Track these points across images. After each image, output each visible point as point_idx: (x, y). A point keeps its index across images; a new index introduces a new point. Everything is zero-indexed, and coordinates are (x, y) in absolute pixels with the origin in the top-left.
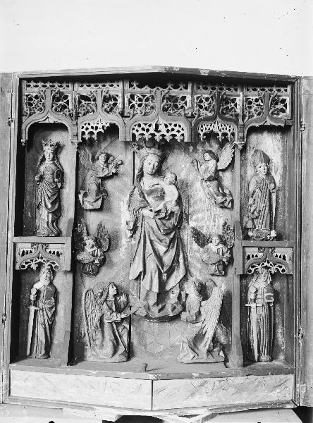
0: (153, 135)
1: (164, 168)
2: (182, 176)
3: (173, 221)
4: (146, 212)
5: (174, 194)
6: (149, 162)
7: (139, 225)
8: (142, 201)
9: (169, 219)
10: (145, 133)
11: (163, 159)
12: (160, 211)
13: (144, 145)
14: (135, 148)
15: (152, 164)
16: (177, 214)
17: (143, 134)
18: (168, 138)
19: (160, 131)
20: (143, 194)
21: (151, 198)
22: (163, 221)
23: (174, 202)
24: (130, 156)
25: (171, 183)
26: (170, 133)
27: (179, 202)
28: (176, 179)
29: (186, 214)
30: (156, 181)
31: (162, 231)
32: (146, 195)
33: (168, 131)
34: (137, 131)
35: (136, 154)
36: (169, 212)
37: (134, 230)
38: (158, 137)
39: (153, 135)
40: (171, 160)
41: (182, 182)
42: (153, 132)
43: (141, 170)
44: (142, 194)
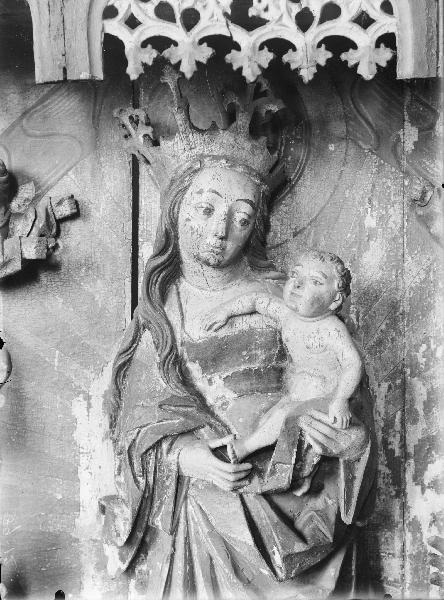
0: (222, 45)
1: (279, 226)
2: (371, 267)
3: (336, 501)
4: (193, 459)
5: (337, 365)
6: (205, 199)
7: (160, 521)
8: (172, 401)
9: (315, 491)
10: (174, 31)
11: (274, 189)
12: (267, 451)
13: (180, 118)
14: (140, 135)
15: (221, 210)
16: (350, 467)
17: (160, 43)
18: (307, 57)
19: (258, 23)
20: (178, 362)
21: (218, 380)
22: (280, 501)
23: (337, 411)
24: (116, 178)
25: (319, 309)
26: (318, 32)
27: (360, 406)
28: (346, 289)
29: (390, 453)
30: (241, 294)
31: (277, 559)
32: (194, 369)
33: (304, 21)
34: (132, 23)
35: (143, 168)
36: (313, 458)
37: (140, 541)
38: (249, 59)
39: (222, 45)
40: (310, 194)
41: (369, 297)
42: (221, 28)
43: (169, 241)
44: (175, 363)
